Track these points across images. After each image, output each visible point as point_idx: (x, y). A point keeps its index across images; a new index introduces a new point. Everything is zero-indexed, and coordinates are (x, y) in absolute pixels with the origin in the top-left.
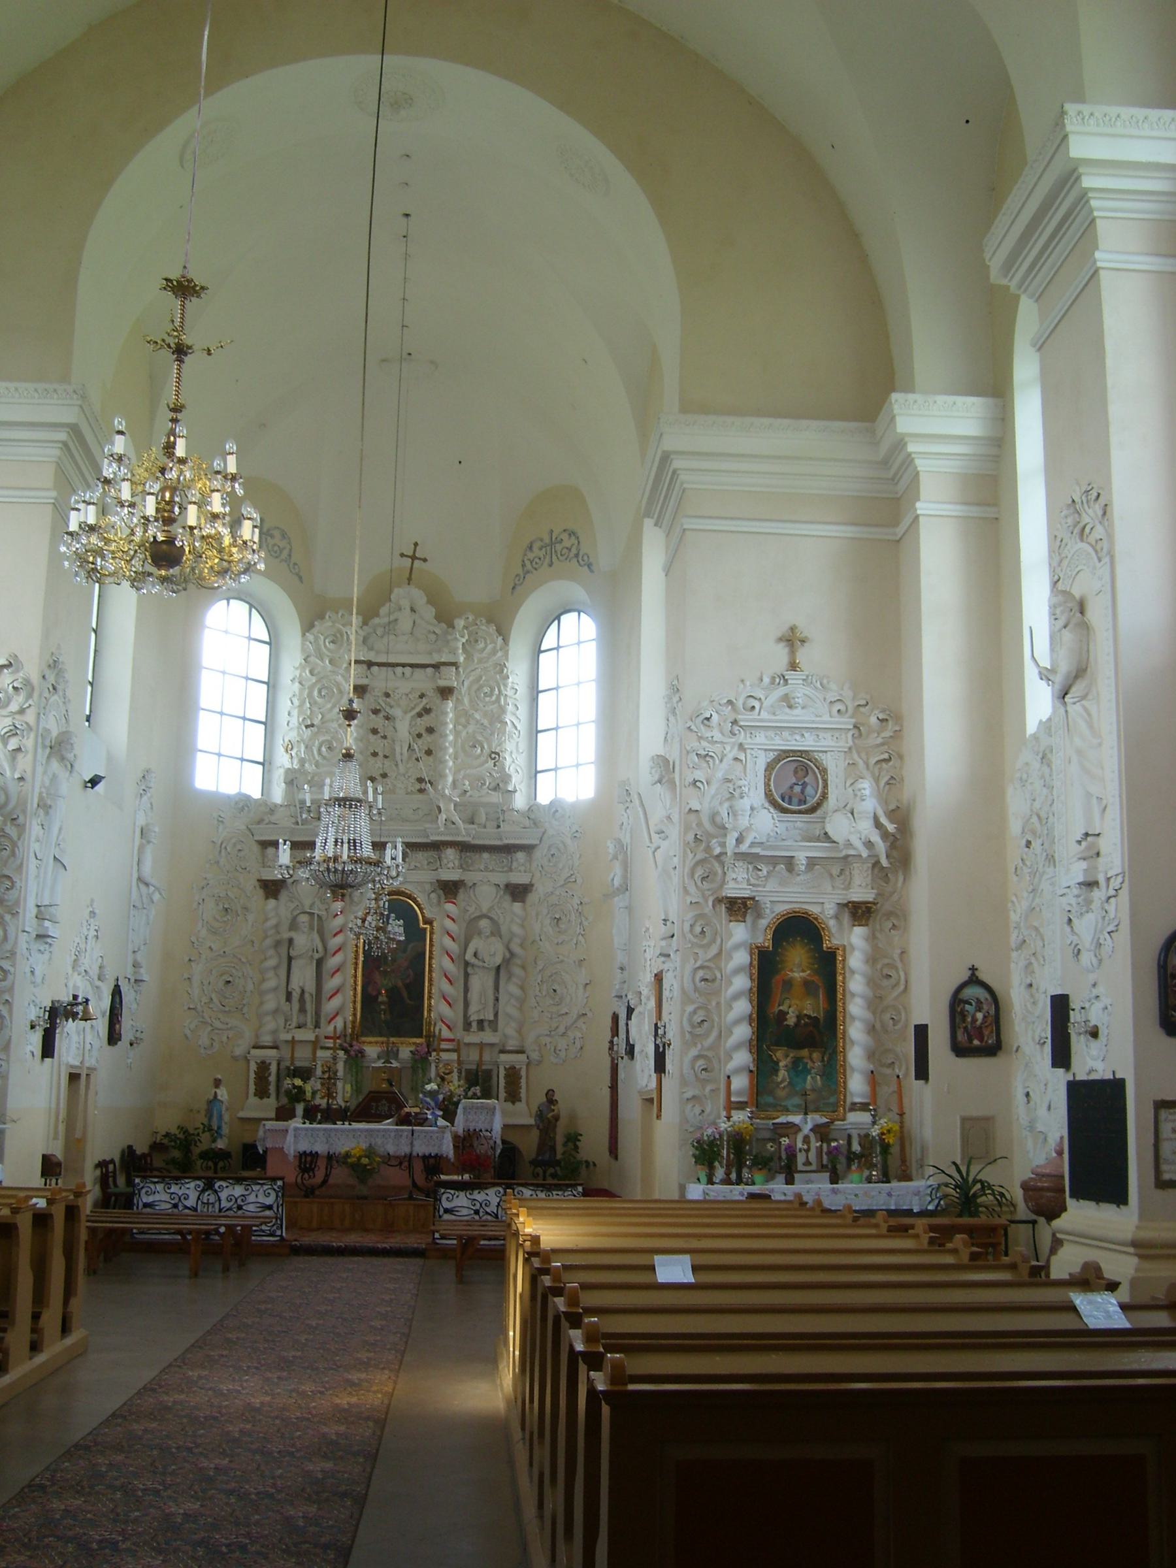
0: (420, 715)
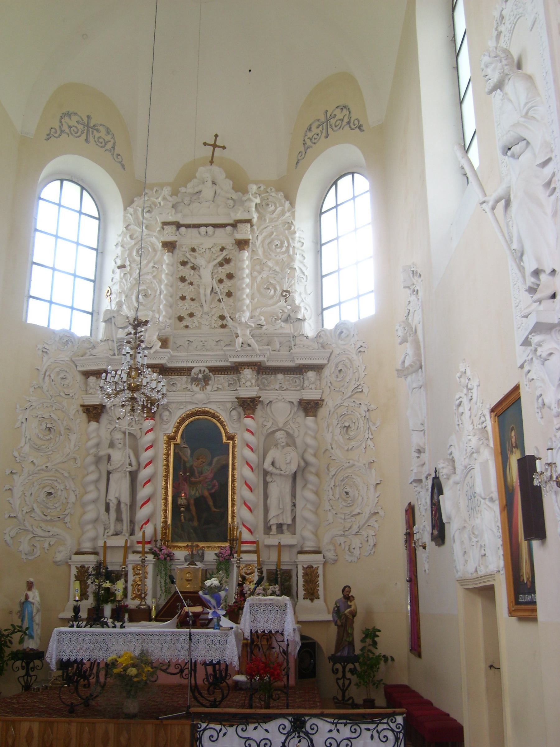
0: (221, 264)
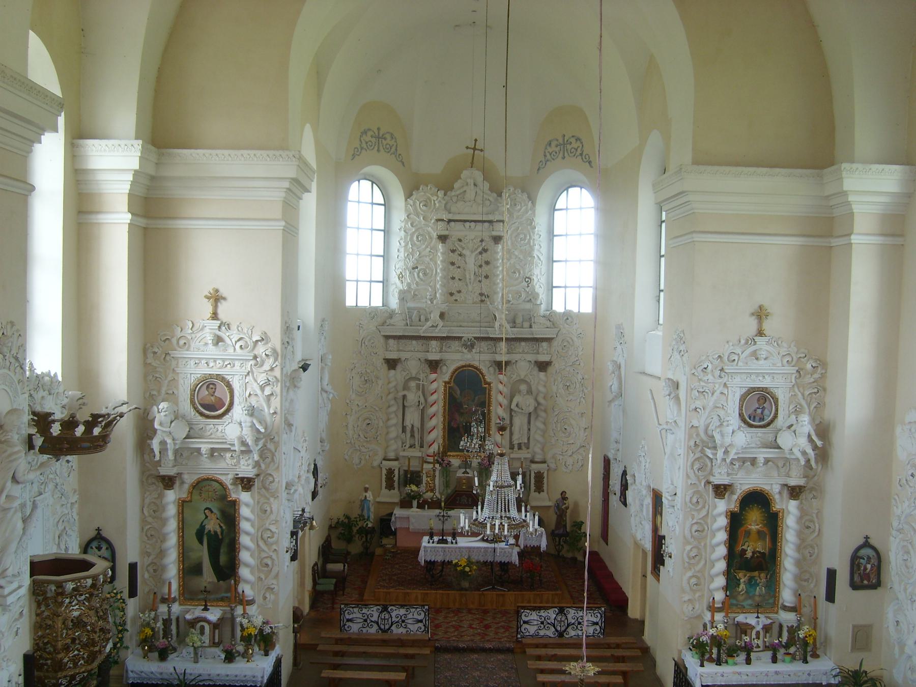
0: (481, 253)
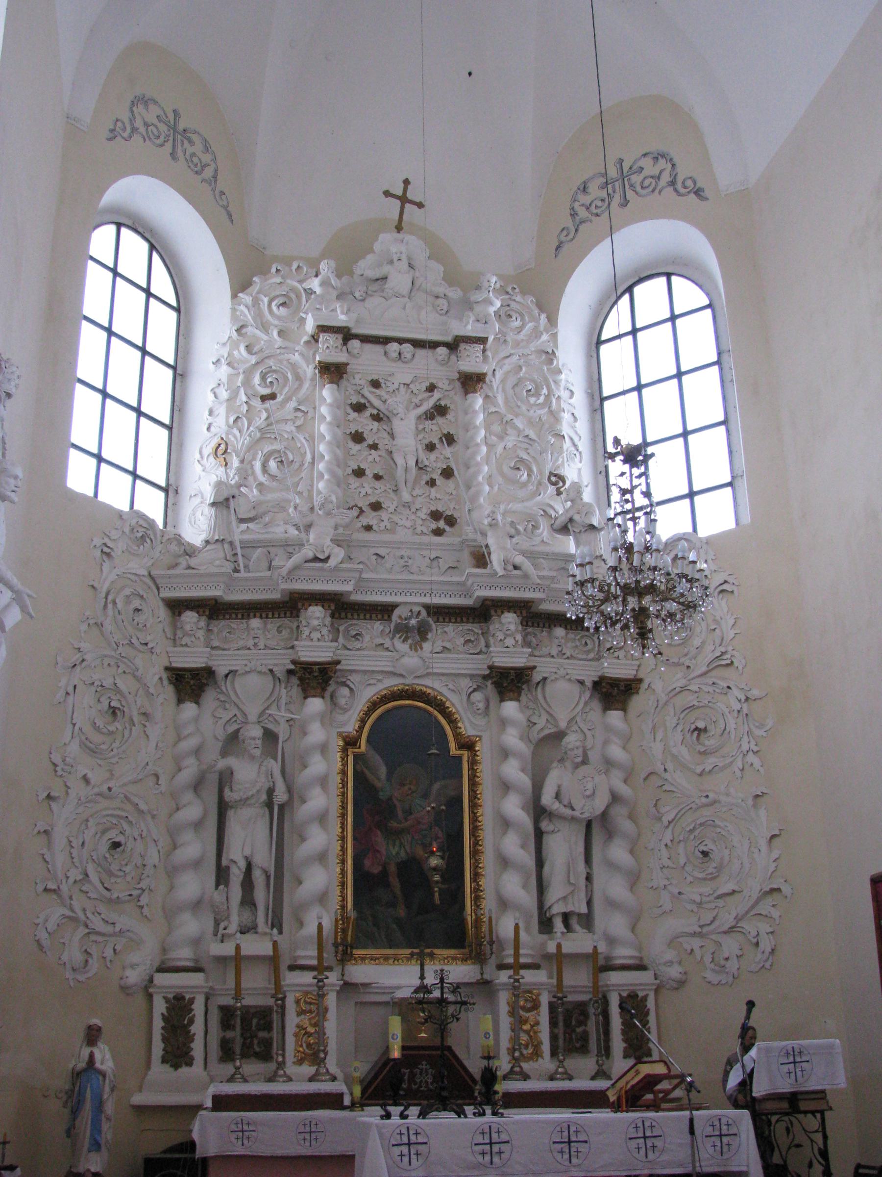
0: (430, 416)
